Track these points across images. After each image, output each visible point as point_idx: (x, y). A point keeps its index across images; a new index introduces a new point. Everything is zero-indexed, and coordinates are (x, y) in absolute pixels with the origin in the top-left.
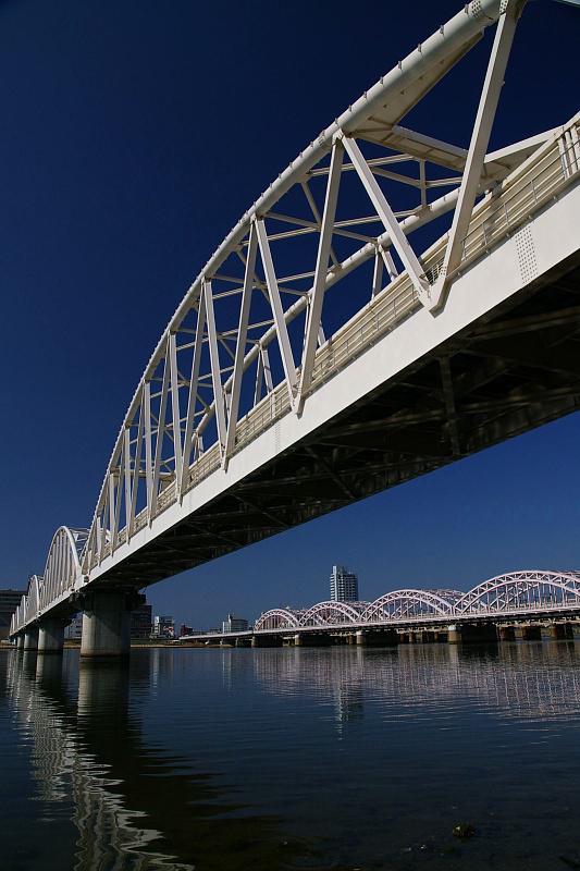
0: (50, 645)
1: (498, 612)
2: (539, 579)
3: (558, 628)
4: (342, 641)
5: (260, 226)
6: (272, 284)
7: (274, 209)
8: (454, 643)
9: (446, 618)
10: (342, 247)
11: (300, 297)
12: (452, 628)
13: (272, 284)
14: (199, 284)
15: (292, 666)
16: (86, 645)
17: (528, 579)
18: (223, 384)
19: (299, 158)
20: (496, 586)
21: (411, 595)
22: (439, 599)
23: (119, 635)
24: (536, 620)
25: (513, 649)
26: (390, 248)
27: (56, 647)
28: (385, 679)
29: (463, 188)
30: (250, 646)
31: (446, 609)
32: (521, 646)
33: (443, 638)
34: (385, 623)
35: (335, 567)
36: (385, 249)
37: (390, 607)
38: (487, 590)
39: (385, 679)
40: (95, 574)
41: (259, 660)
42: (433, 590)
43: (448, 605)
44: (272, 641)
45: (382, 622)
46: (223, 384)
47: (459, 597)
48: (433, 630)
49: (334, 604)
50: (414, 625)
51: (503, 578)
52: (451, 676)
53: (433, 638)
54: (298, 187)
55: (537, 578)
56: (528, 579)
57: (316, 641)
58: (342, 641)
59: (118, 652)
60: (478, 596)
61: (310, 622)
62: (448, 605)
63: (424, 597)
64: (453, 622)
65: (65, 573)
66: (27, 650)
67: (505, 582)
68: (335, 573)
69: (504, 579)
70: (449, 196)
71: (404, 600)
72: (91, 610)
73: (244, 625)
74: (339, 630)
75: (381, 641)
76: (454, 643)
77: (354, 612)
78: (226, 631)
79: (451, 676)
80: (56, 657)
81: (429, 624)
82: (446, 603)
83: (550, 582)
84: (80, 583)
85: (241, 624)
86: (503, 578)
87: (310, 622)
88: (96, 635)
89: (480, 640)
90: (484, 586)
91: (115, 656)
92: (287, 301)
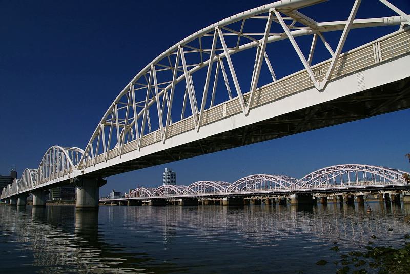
0: (39, 203)
1: (245, 192)
2: (265, 179)
3: (270, 200)
4: (170, 204)
5: (154, 68)
6: (156, 85)
7: (137, 82)
8: (225, 205)
9: (222, 194)
10: (178, 75)
11: (252, 41)
12: (225, 199)
13: (156, 85)
14: (129, 86)
15: (147, 214)
16: (34, 203)
17: (260, 178)
18: (137, 114)
19: (201, 30)
20: (246, 180)
21: (207, 183)
22: (220, 185)
23: (94, 198)
24: (324, 193)
25: (249, 208)
26: (224, 59)
27: (42, 204)
28: (194, 220)
29: (172, 83)
30: (119, 205)
31: (224, 190)
32: (252, 207)
33: (177, 203)
34: (193, 196)
35: (166, 169)
36: (221, 59)
37: (196, 189)
38: (242, 182)
39: (194, 220)
40: (37, 187)
41: (128, 211)
42: (279, 175)
43: (224, 189)
44: (137, 203)
45: (192, 195)
46: (137, 114)
47: (228, 185)
48: (214, 199)
49: (165, 186)
50: (204, 197)
51: (250, 177)
52: (223, 219)
53: (214, 203)
54: (143, 76)
55: (347, 168)
56: (260, 178)
57: (159, 203)
58: (170, 204)
59: (94, 206)
60: (238, 185)
61: (157, 194)
62: (224, 189)
63: (212, 184)
64: (225, 196)
65: (29, 185)
66: (19, 205)
67: (250, 179)
68: (166, 172)
69: (250, 177)
70: (170, 85)
71: (203, 185)
72: (80, 186)
73: (119, 195)
74: (169, 198)
75: (191, 203)
76: (225, 205)
77: (221, 187)
78: (111, 198)
79: (223, 219)
80: (42, 209)
81: (211, 197)
82: (223, 188)
83: (270, 180)
84: (33, 188)
85: (119, 195)
86: (241, 180)
87: (157, 194)
88: (84, 198)
89: (237, 203)
90: (241, 180)
91: (93, 208)
92: (160, 91)
